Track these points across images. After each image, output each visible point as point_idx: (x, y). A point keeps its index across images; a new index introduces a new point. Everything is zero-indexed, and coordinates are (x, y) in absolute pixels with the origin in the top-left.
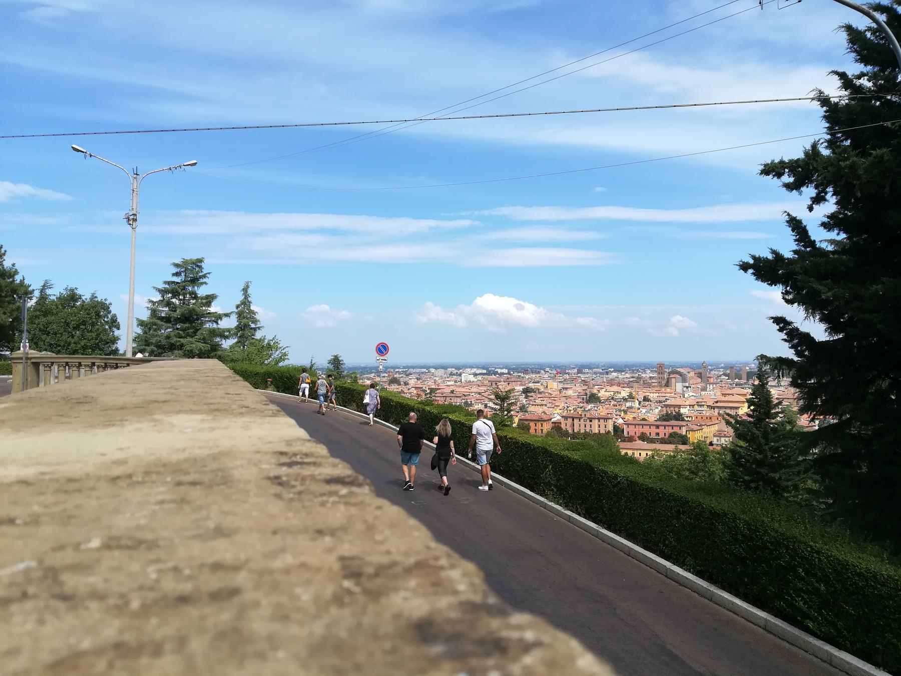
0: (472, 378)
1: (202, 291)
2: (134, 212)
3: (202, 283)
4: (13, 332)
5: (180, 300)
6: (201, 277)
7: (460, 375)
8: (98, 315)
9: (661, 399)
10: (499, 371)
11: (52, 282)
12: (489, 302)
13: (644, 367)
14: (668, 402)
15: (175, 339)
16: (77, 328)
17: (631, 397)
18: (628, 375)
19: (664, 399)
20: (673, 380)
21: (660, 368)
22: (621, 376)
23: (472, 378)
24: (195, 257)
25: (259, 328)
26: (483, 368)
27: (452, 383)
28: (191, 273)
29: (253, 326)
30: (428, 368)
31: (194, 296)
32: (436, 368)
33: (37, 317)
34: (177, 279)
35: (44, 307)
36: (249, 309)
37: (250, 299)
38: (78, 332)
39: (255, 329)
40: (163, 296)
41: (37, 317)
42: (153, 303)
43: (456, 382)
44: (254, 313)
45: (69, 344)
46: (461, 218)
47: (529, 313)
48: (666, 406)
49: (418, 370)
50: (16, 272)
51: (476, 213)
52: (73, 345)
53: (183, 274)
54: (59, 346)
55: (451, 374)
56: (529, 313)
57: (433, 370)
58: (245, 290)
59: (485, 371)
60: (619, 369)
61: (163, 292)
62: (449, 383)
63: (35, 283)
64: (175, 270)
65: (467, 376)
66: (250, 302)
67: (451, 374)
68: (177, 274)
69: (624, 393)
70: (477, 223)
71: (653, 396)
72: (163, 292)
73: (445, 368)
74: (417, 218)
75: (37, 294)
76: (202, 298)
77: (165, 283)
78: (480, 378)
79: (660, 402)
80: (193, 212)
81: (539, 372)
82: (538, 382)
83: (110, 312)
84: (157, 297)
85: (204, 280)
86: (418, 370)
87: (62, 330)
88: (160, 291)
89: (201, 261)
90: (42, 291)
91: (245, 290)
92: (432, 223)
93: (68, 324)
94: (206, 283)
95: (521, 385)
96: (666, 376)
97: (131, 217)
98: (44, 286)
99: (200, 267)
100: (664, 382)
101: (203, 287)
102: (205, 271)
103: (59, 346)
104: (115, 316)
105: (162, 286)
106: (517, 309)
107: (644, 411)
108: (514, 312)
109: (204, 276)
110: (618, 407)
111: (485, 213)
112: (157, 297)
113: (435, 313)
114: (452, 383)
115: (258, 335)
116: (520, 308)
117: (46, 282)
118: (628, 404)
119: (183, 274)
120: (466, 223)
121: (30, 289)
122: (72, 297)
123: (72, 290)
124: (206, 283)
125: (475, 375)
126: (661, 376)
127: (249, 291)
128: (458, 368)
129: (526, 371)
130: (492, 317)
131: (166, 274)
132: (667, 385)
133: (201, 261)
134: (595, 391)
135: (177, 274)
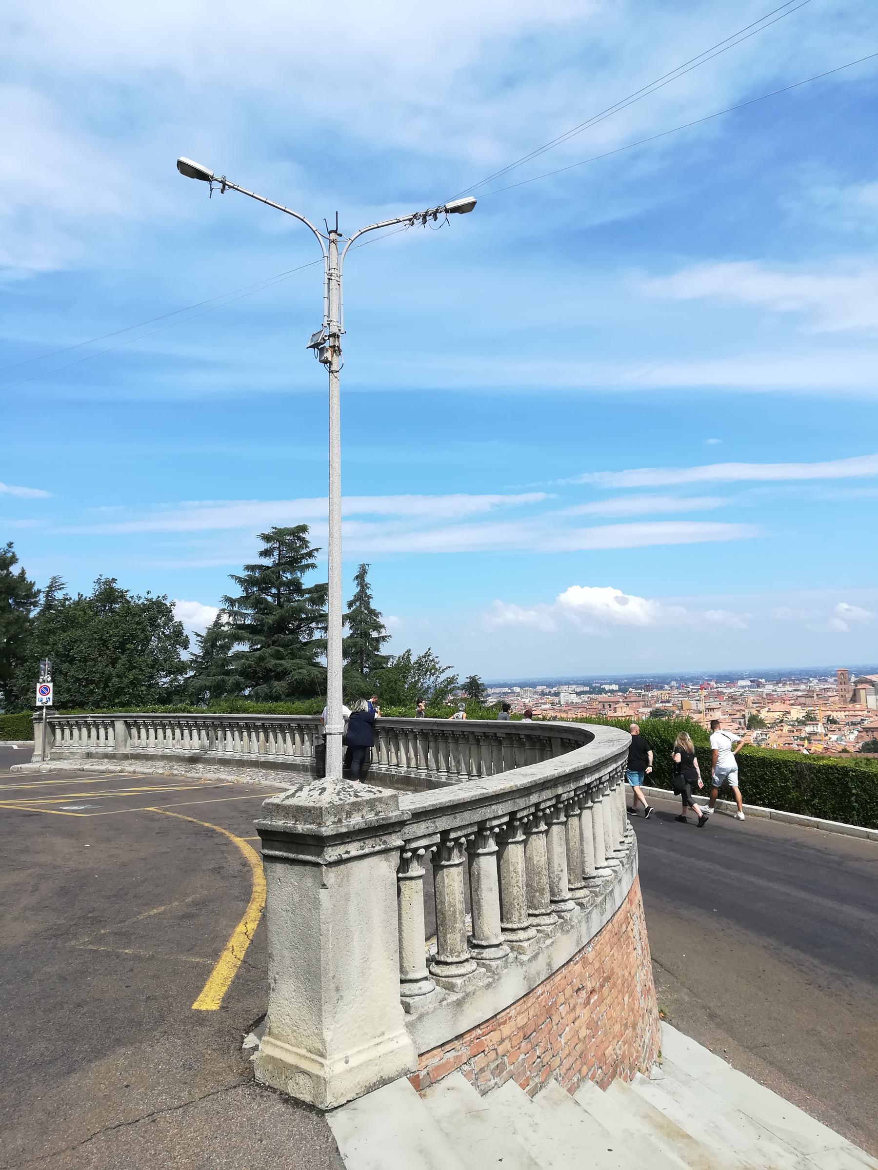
0: (574, 698)
1: (309, 580)
2: (334, 329)
3: (308, 566)
4: (8, 660)
5: (273, 596)
6: (303, 557)
7: (557, 694)
8: (153, 621)
9: (854, 720)
10: (607, 687)
11: (62, 580)
12: (576, 596)
13: (822, 676)
14: (866, 724)
15: (274, 662)
16: (122, 646)
17: (810, 719)
18: (788, 688)
19: (859, 719)
20: (862, 692)
21: (842, 676)
22: (780, 689)
23: (574, 698)
24: (293, 525)
25: (384, 638)
26: (585, 685)
27: (548, 706)
28: (289, 547)
29: (374, 634)
30: (510, 686)
31: (295, 586)
32: (522, 686)
33: (52, 632)
34: (268, 562)
35: (67, 617)
36: (368, 608)
37: (368, 592)
38: (112, 655)
39: (377, 640)
40: (246, 590)
41: (52, 632)
42: (231, 601)
43: (553, 704)
44: (377, 615)
45: (109, 678)
46: (531, 490)
47: (637, 608)
48: (867, 730)
49: (497, 690)
50: (14, 560)
51: (550, 483)
52: (115, 680)
53: (276, 553)
54: (92, 682)
55: (543, 694)
56: (637, 608)
57: (517, 689)
58: (361, 577)
59: (587, 689)
60: (778, 678)
61: (246, 583)
62: (543, 707)
63: (41, 584)
64: (264, 546)
65: (567, 696)
66: (369, 597)
67: (543, 694)
68: (266, 553)
69: (797, 713)
70: (553, 496)
71: (839, 716)
72: (246, 583)
73: (533, 685)
74: (472, 493)
75: (42, 598)
76: (309, 591)
77: (248, 568)
78: (585, 698)
79: (853, 724)
80: (196, 503)
81: (662, 688)
82: (668, 702)
83: (171, 619)
84: (237, 592)
85: (311, 561)
86: (497, 690)
87: (96, 654)
88: (241, 581)
89: (303, 529)
90: (48, 594)
91: (361, 577)
92: (495, 499)
93: (104, 642)
94: (313, 566)
95: (644, 706)
96: (852, 686)
97: (329, 343)
98: (50, 587)
99: (305, 542)
100: (849, 696)
101: (309, 572)
102: (312, 547)
103: (92, 682)
104: (180, 624)
105: (244, 574)
106: (618, 602)
107: (834, 738)
108: (616, 607)
109: (310, 555)
110: (796, 733)
111: (562, 482)
112: (237, 592)
113: (512, 614)
114: (548, 706)
115: (385, 650)
116: (622, 602)
117: (54, 580)
118: (809, 729)
119: (276, 553)
120: (540, 496)
121: (35, 588)
122: (109, 594)
123: (109, 582)
124: (313, 566)
125: (578, 694)
126: (843, 687)
127: (367, 579)
128: (550, 685)
129: (648, 687)
130: (586, 614)
131: (251, 553)
132: (854, 699)
133: (303, 529)
134: (754, 712)
135: (266, 553)
